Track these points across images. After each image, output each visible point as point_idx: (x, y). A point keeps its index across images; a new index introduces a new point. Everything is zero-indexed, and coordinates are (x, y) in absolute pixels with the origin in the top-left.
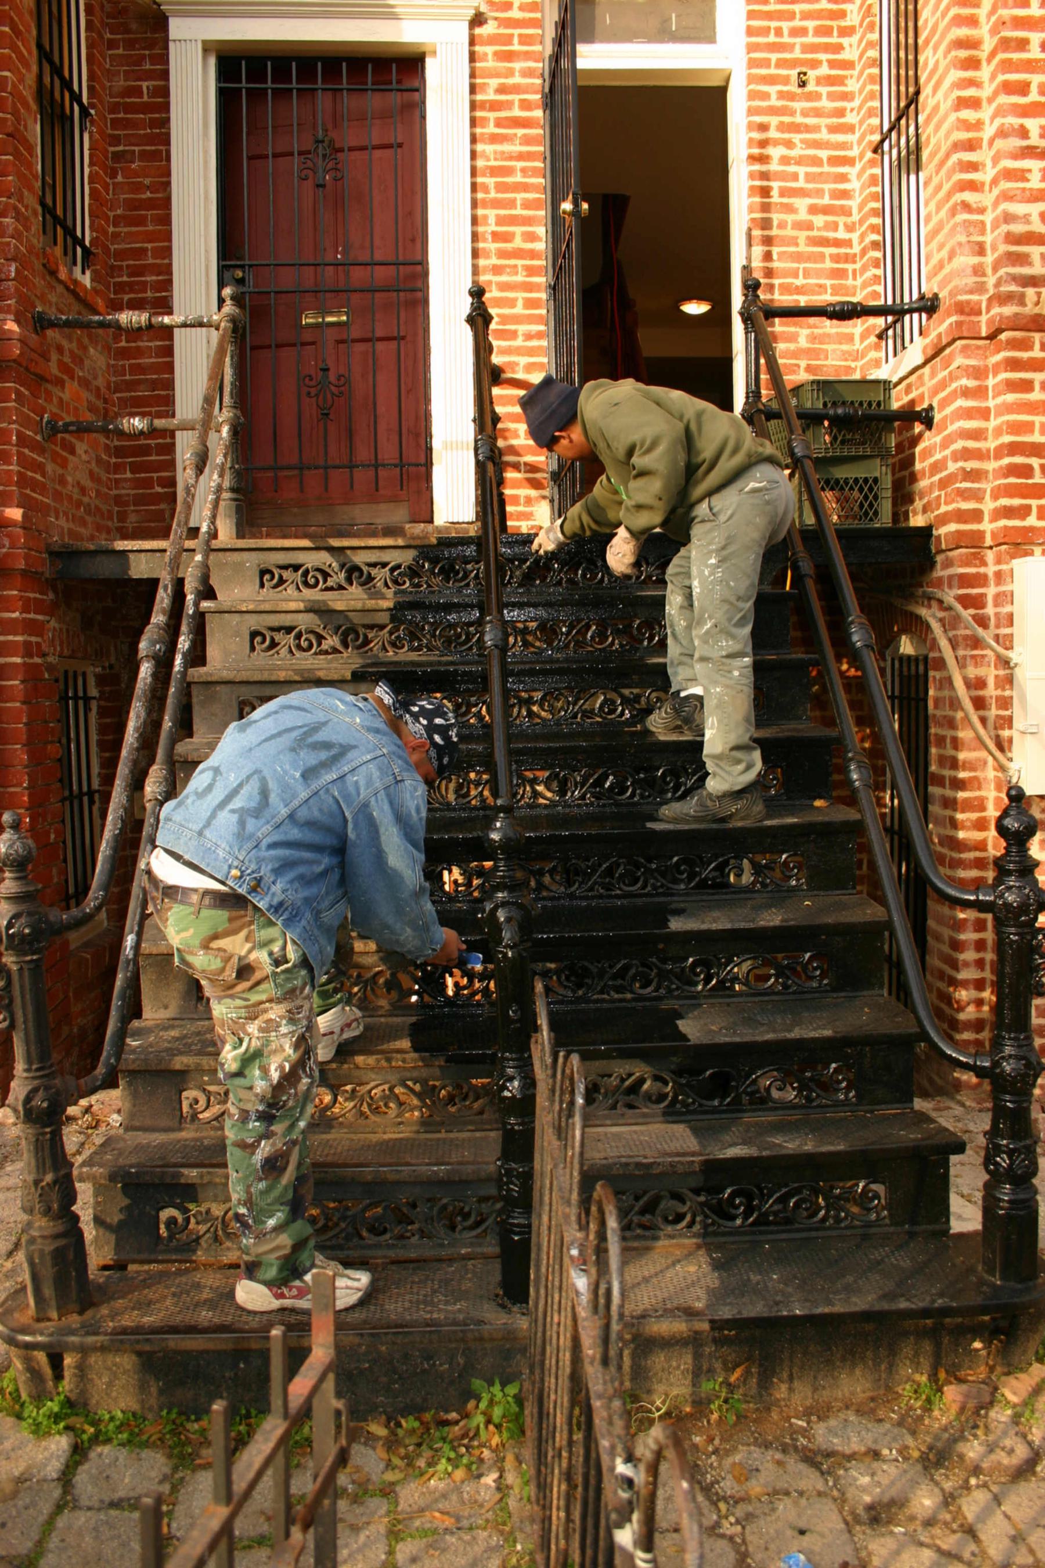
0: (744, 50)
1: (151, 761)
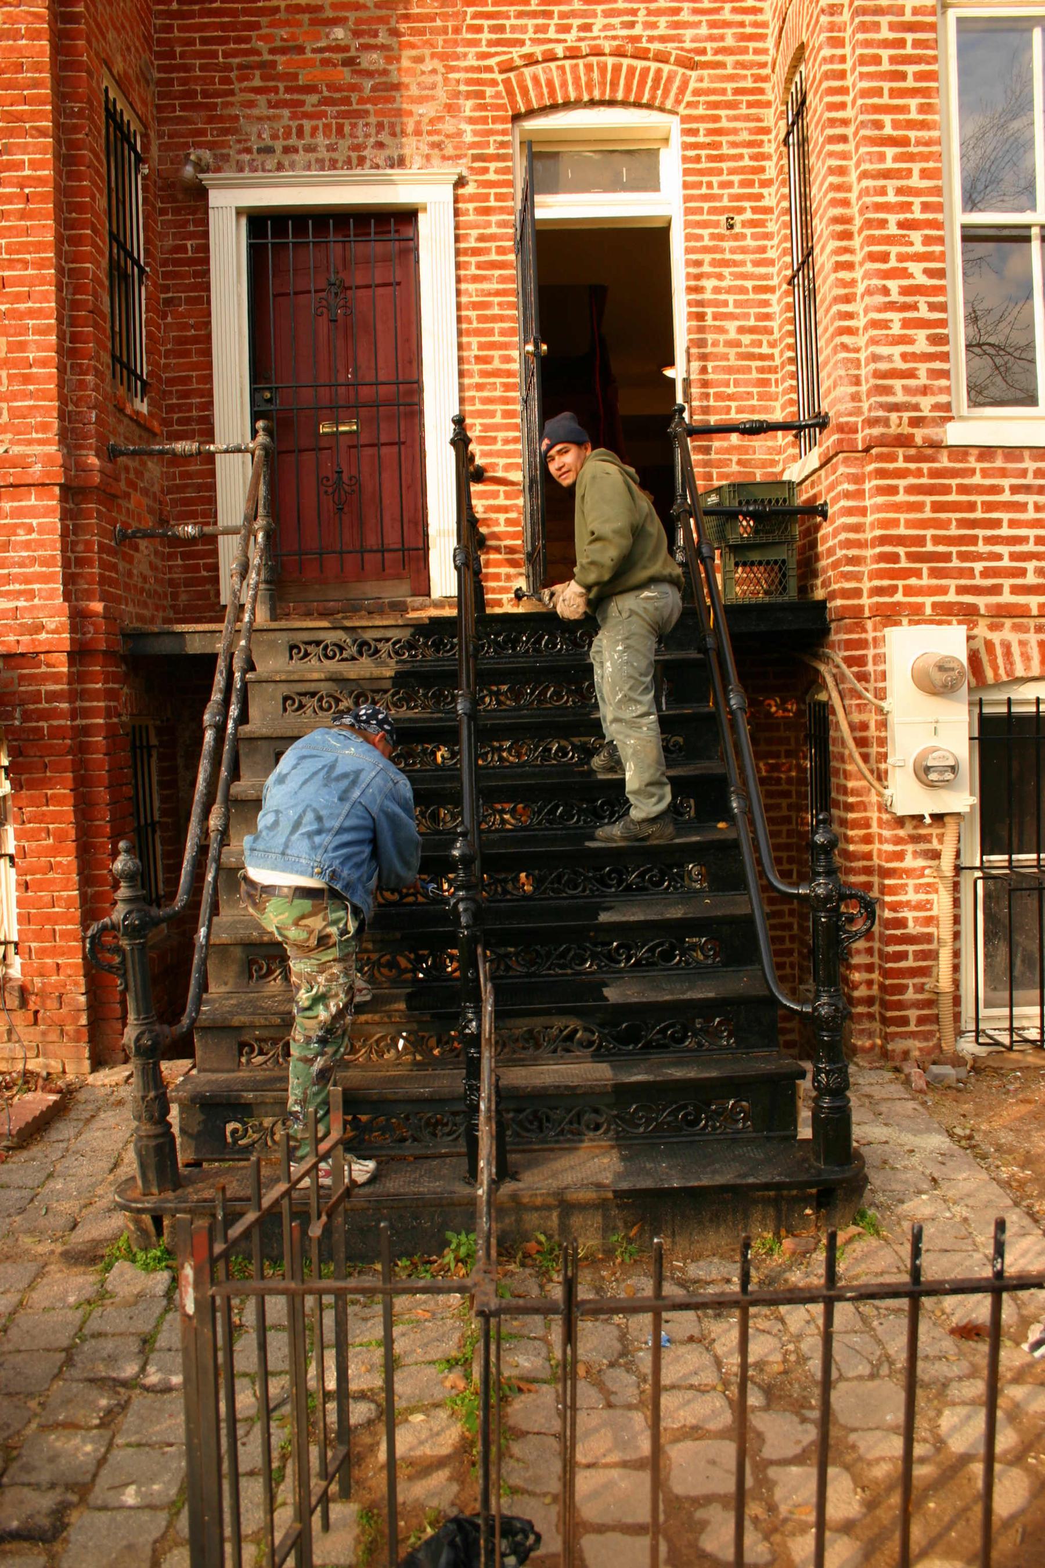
0: (681, 200)
1: (213, 802)
